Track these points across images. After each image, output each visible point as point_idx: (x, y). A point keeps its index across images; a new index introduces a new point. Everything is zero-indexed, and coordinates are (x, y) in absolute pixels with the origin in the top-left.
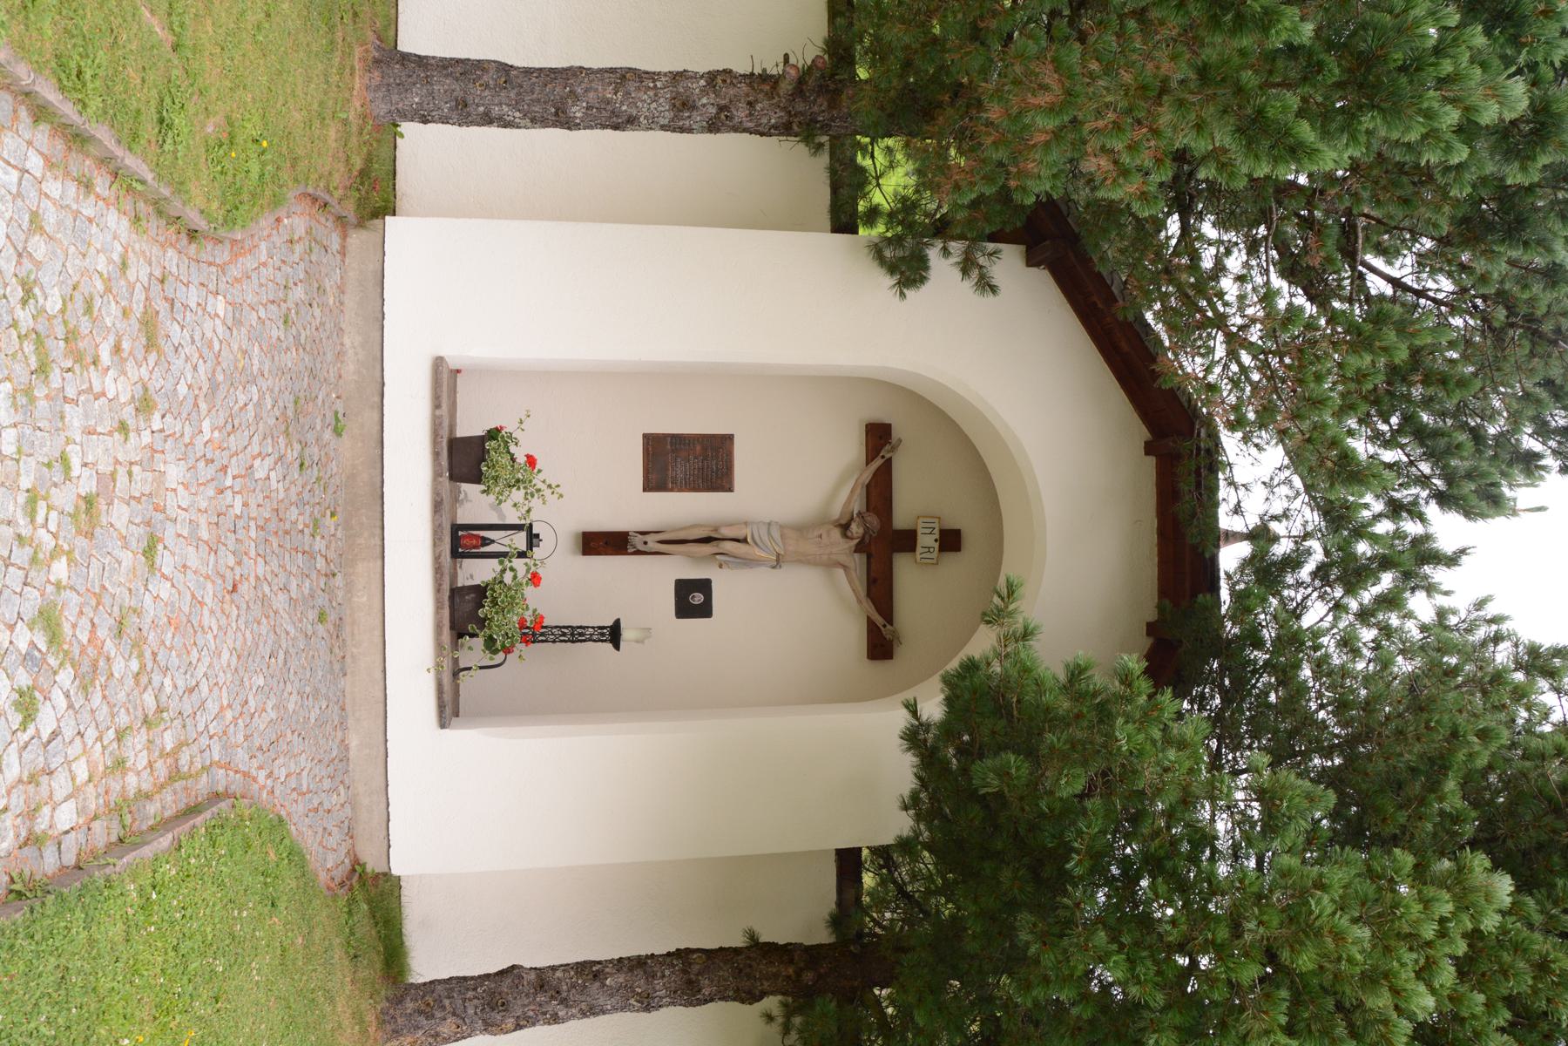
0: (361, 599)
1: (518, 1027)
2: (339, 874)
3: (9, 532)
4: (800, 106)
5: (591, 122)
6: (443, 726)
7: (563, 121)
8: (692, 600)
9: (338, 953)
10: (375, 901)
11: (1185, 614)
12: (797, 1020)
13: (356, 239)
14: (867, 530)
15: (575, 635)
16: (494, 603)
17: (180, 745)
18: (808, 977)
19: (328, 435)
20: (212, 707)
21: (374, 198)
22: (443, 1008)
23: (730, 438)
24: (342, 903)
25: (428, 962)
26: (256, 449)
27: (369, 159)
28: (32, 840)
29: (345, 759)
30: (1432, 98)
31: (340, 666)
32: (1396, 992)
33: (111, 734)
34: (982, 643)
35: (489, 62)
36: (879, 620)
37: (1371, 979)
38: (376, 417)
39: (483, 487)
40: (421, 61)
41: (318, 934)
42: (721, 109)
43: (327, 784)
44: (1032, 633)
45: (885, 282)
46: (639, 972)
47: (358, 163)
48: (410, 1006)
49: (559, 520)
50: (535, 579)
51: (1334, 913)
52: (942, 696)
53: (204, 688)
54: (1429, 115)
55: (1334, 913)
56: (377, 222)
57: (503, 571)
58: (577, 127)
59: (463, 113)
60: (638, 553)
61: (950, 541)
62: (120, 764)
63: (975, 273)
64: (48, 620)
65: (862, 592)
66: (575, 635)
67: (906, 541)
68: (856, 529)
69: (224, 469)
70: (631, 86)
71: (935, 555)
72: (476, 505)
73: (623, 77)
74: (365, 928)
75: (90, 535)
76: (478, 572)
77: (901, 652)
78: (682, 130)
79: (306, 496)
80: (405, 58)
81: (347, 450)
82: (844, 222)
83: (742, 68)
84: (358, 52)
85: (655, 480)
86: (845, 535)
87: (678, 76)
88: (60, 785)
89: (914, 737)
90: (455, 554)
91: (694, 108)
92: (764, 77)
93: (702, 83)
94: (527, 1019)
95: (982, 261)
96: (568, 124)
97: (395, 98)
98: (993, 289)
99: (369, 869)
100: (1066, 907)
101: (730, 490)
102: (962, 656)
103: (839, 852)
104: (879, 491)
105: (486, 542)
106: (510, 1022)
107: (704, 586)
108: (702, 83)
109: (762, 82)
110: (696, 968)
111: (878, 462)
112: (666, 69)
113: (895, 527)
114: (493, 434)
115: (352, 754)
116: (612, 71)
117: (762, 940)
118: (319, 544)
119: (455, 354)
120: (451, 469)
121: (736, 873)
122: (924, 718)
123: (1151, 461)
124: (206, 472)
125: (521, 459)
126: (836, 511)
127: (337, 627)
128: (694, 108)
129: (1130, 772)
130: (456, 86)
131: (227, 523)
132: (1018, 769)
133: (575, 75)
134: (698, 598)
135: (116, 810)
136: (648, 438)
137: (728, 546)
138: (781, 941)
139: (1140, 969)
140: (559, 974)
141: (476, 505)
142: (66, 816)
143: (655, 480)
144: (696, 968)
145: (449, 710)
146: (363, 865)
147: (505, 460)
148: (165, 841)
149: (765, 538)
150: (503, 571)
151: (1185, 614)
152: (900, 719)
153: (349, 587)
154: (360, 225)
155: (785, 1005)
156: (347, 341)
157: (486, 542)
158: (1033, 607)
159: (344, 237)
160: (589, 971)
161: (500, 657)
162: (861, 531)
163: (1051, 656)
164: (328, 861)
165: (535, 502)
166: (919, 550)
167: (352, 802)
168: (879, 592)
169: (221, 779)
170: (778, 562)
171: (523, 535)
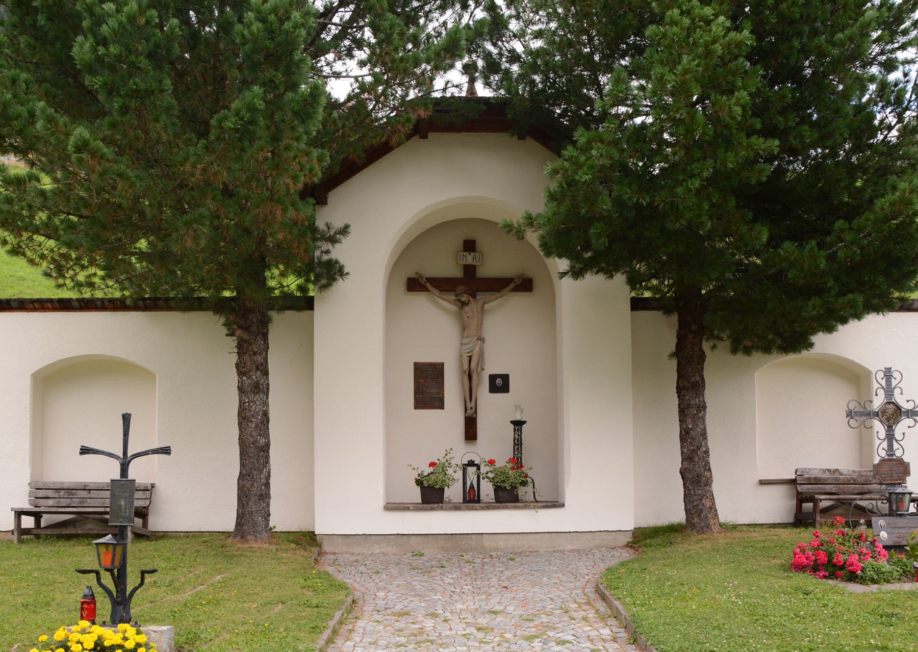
0: (501, 544)
1: (709, 470)
2: (632, 551)
3: (497, 649)
4: (254, 328)
5: (266, 435)
6: (563, 505)
7: (266, 448)
8: (500, 384)
9: (668, 549)
10: (644, 538)
11: (518, 119)
12: (716, 333)
13: (327, 548)
14: (465, 292)
15: (518, 444)
16: (503, 481)
17: (575, 602)
18: (694, 327)
19: (424, 558)
20: (558, 593)
21: (308, 539)
22: (698, 505)
23: (415, 364)
24: (646, 549)
25: (679, 516)
26: (440, 583)
27: (293, 542)
28: (615, 640)
29: (578, 551)
30: (287, 25)
31: (535, 553)
32: (714, 42)
33: (573, 622)
34: (533, 237)
35: (238, 484)
36: (512, 286)
37: (708, 53)
38: (413, 537)
39: (446, 488)
40: (240, 517)
41: (660, 556)
42: (258, 369)
43: (590, 556)
44: (529, 215)
45: (340, 285)
46: (686, 411)
47: (293, 546)
48: (696, 520)
49: (461, 452)
50: (492, 462)
51: (675, 74)
52: (556, 258)
53: (550, 596)
54: (295, 27)
55: (675, 74)
56: (318, 538)
57: (488, 477)
58: (269, 441)
59: (265, 496)
60: (476, 412)
61: (470, 246)
62: (585, 619)
63: (338, 236)
64: (530, 638)
65: (498, 294)
66: (518, 444)
67: (470, 270)
68: (464, 298)
69: (453, 592)
70: (249, 414)
71: (477, 255)
72: (454, 493)
73: (244, 418)
74: (659, 540)
75: (492, 629)
76: (487, 490)
77: (529, 273)
78: (268, 389)
79: (456, 565)
80: (238, 524)
81: (430, 551)
82: (308, 304)
83: (234, 358)
84: (239, 545)
85: (438, 403)
86: (468, 304)
87: (241, 390)
88: (593, 634)
89: (576, 273)
90: (478, 501)
91: (258, 382)
92: (240, 346)
93: (245, 378)
94: (706, 465)
95: (332, 233)
96: (268, 445)
97: (260, 529)
98: (347, 227)
99: (630, 540)
100: (664, 208)
101: (443, 364)
102: (539, 250)
103: (633, 309)
104: (442, 285)
105: (472, 487)
106: (706, 473)
107: (493, 378)
108: (245, 378)
109: (242, 348)
110: (686, 384)
111: (428, 286)
112: (237, 398)
113: (460, 274)
114: (419, 482)
115: (575, 548)
116: (240, 424)
117: (674, 350)
118: (477, 560)
119: (381, 504)
120: (438, 503)
121: (640, 363)
122: (568, 268)
123: (431, 135)
124: (455, 597)
125: (431, 469)
126: (453, 308)
127: (517, 552)
128: (258, 382)
129: (602, 168)
130: (253, 500)
131: (476, 591)
132: (597, 229)
133: (244, 442)
134: (499, 381)
135: (603, 619)
136: (417, 407)
137: (473, 365)
138: (675, 340)
139: (696, 171)
140: (685, 450)
141: (454, 493)
142: (606, 632)
143: (438, 403)
144: (686, 384)
145: (556, 504)
146: (629, 543)
147: (433, 477)
148: (617, 603)
149: (469, 346)
150: (488, 477)
151: (518, 119)
152: (568, 281)
153: (495, 549)
154: (319, 546)
155: (707, 340)
156: (377, 552)
157: (472, 487)
158: (517, 216)
159: (327, 553)
160: (685, 436)
161: (529, 480)
162: (465, 295)
163: (539, 206)
164: (627, 554)
165: (453, 462)
166: (474, 263)
167: (599, 547)
168: (498, 285)
169: (590, 590)
170: (481, 339)
171: (469, 468)
